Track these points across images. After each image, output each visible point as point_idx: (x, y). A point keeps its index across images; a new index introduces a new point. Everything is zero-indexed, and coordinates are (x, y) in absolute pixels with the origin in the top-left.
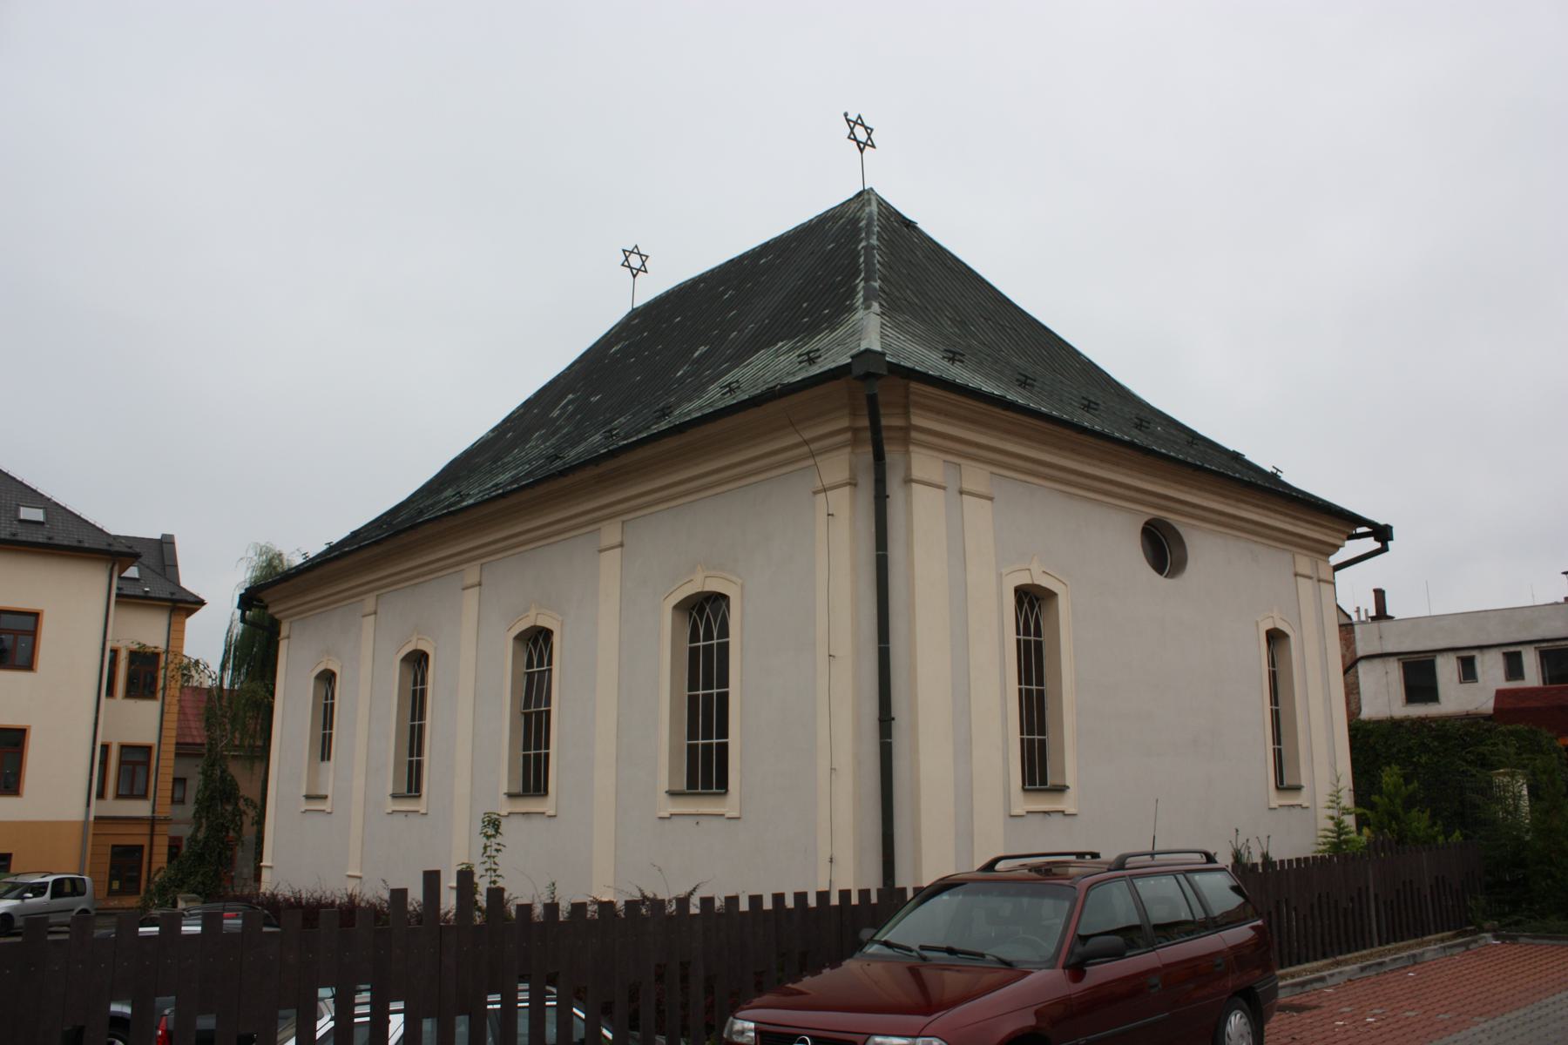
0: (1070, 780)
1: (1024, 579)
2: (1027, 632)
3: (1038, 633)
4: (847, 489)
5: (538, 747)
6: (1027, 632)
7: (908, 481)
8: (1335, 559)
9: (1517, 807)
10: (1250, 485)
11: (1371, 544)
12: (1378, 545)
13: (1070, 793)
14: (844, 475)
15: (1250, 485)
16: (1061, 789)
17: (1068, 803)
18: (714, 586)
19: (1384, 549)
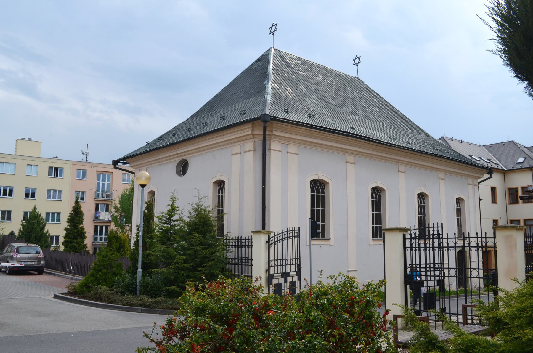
0: (331, 237)
1: (375, 185)
2: (421, 203)
3: (424, 203)
4: (253, 152)
5: (376, 227)
6: (421, 203)
7: (270, 149)
8: (479, 180)
9: (157, 256)
10: (464, 162)
11: (487, 176)
12: (489, 176)
13: (331, 241)
14: (252, 148)
15: (464, 162)
16: (329, 239)
17: (330, 242)
18: (222, 178)
19: (491, 177)
